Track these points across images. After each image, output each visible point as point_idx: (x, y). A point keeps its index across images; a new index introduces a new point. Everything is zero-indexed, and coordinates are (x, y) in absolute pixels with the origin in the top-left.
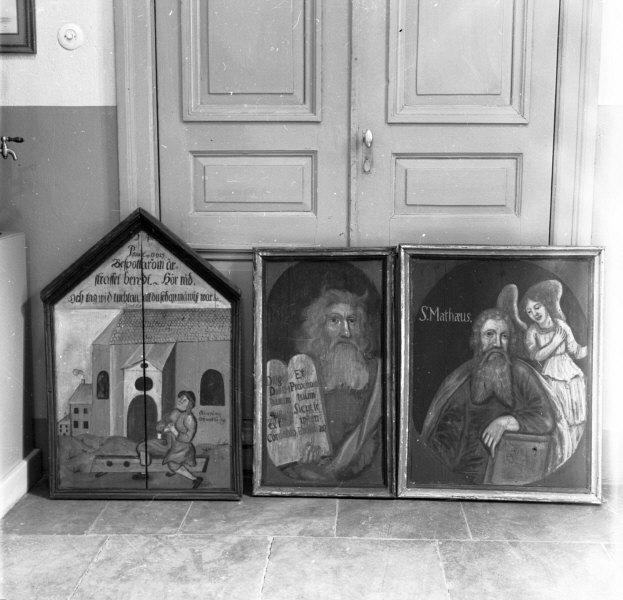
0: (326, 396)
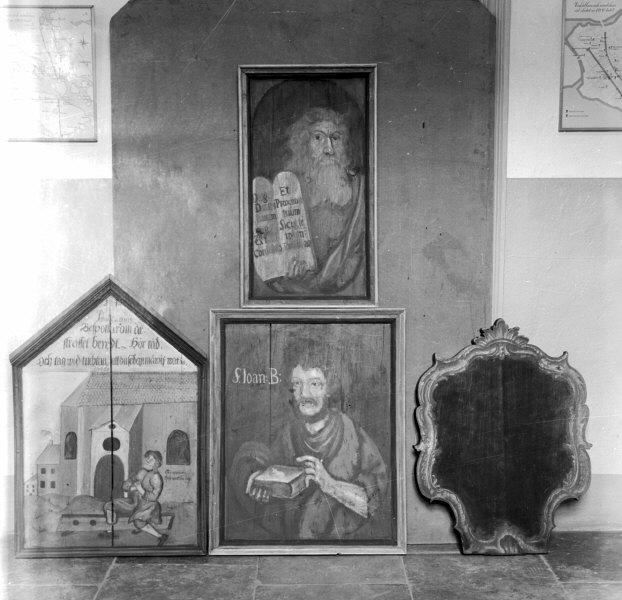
0: (309, 212)
